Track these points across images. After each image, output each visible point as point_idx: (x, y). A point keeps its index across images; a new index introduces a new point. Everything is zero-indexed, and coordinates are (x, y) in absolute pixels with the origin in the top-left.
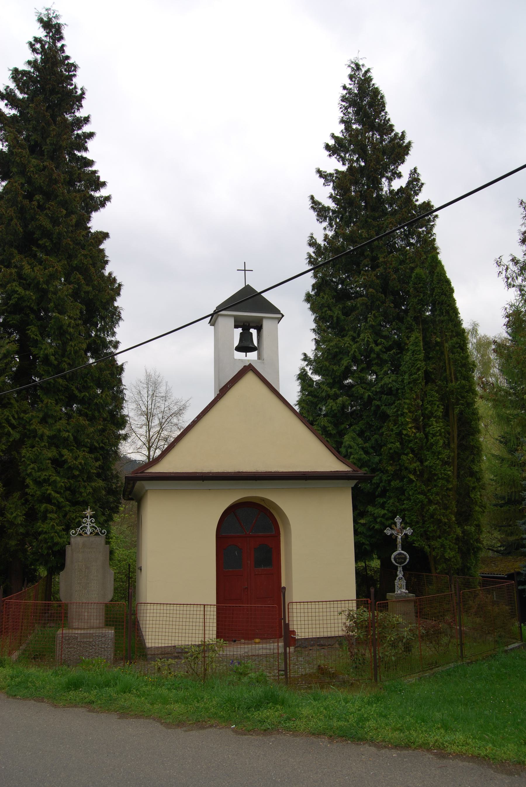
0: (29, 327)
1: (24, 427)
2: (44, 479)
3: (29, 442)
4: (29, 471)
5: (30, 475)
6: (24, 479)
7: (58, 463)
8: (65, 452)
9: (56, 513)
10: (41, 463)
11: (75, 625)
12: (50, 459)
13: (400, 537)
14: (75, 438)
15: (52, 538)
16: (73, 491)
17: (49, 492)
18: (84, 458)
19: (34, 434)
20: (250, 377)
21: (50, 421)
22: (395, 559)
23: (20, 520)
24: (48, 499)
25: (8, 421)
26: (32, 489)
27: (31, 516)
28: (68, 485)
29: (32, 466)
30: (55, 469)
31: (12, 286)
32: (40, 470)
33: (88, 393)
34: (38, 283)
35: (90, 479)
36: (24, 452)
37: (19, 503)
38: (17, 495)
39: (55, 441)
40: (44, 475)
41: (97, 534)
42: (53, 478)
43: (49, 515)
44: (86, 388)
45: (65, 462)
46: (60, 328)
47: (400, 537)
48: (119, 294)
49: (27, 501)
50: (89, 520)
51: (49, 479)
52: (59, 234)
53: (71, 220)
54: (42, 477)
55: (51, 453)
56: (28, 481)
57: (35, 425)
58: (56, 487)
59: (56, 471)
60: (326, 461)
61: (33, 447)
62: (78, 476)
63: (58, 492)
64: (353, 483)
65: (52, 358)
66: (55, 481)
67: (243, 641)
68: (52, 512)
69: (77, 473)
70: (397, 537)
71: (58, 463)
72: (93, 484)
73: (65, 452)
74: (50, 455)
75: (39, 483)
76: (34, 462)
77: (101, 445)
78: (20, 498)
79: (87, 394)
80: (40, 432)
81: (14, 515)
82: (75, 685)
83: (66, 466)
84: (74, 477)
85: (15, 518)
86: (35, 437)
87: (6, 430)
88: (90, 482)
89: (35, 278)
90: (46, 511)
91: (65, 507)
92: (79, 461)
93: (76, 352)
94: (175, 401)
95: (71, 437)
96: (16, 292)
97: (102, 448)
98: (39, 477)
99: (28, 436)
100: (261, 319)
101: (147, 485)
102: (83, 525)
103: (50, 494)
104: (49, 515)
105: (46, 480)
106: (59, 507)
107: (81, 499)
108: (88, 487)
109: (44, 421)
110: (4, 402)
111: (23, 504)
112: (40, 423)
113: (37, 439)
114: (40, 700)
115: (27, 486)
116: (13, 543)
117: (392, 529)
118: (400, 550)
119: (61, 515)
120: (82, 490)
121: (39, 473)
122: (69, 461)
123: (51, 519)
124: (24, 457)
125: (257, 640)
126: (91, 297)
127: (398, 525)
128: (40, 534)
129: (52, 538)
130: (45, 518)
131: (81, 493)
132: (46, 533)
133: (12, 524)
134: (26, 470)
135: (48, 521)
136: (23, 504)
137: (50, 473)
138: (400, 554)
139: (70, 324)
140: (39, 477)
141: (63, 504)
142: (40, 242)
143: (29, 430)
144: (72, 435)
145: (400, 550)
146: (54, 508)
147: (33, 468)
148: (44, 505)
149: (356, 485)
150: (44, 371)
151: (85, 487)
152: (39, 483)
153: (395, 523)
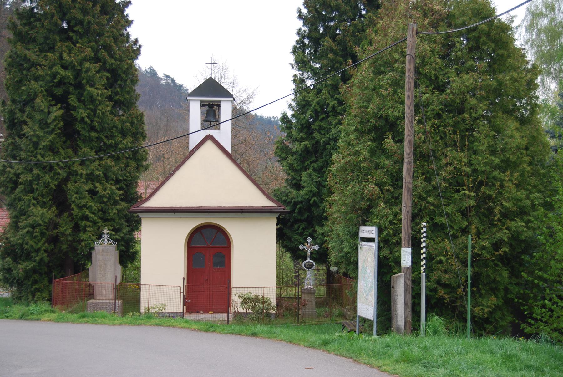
0: (71, 96)
1: (69, 168)
2: (84, 205)
3: (73, 178)
4: (73, 199)
5: (74, 202)
6: (70, 205)
7: (93, 192)
8: (98, 185)
9: (92, 227)
10: (81, 193)
11: (98, 297)
12: (86, 191)
13: (309, 251)
14: (105, 175)
15: (90, 244)
16: (104, 211)
17: (87, 213)
18: (111, 189)
19: (76, 173)
20: (209, 143)
21: (88, 163)
22: (305, 266)
23: (69, 231)
24: (86, 218)
25: (58, 164)
26: (76, 211)
27: (76, 228)
28: (100, 208)
29: (76, 195)
30: (91, 197)
31: (56, 69)
32: (80, 198)
33: (114, 140)
34: (74, 66)
35: (116, 203)
36: (69, 186)
37: (68, 220)
38: (66, 214)
39: (91, 177)
40: (83, 202)
41: (111, 244)
42: (89, 204)
43: (88, 229)
44: (112, 137)
45: (98, 192)
46: (91, 97)
47: (309, 251)
48: (139, 53)
49: (73, 219)
50: (106, 236)
51: (86, 205)
52: (89, 23)
53: (96, 10)
54: (82, 204)
55: (88, 186)
56: (73, 206)
57: (76, 167)
58: (91, 209)
59: (92, 198)
60: (260, 200)
61: (76, 182)
62: (107, 202)
63: (93, 213)
64: (277, 215)
65: (87, 119)
66: (91, 206)
67: (202, 312)
68: (89, 227)
69: (105, 200)
70: (307, 251)
71: (93, 192)
72: (118, 207)
73: (98, 185)
74: (87, 188)
75: (80, 207)
76: (77, 193)
77: (124, 178)
78: (68, 217)
79: (113, 142)
80: (79, 172)
81: (65, 228)
82: (84, 317)
83: (98, 195)
84: (104, 203)
85: (65, 230)
86: (77, 175)
87: (57, 171)
88: (116, 205)
89: (72, 62)
90: (86, 226)
91: (98, 222)
92: (107, 192)
93: (103, 113)
94: (243, 89)
95: (102, 175)
96: (59, 73)
97: (125, 180)
98: (80, 203)
99: (71, 174)
100: (219, 101)
101: (141, 215)
102: (103, 239)
103: (87, 215)
104: (88, 229)
105: (85, 206)
106: (94, 223)
107: (109, 217)
108: (114, 209)
109: (82, 163)
110: (55, 151)
111: (71, 221)
112: (81, 164)
113: (78, 177)
114: (68, 322)
115: (73, 209)
116: (64, 247)
117: (304, 245)
118: (309, 260)
119: (96, 228)
120: (110, 211)
121: (80, 201)
122: (100, 192)
123: (89, 231)
124: (70, 189)
125: (211, 312)
126: (114, 67)
127: (309, 243)
128: (82, 240)
129: (90, 244)
130: (85, 231)
131: (109, 213)
132: (85, 240)
133: (63, 234)
134: (71, 198)
135: (87, 232)
136: (71, 221)
137: (87, 200)
138: (309, 262)
139: (98, 94)
140: (80, 203)
141: (97, 221)
142: (75, 29)
143: (73, 170)
144: (103, 173)
145: (309, 260)
146: (91, 224)
147: (76, 198)
148: (84, 222)
149: (279, 216)
150: (82, 128)
151: (112, 209)
152: (80, 207)
153: (307, 242)
